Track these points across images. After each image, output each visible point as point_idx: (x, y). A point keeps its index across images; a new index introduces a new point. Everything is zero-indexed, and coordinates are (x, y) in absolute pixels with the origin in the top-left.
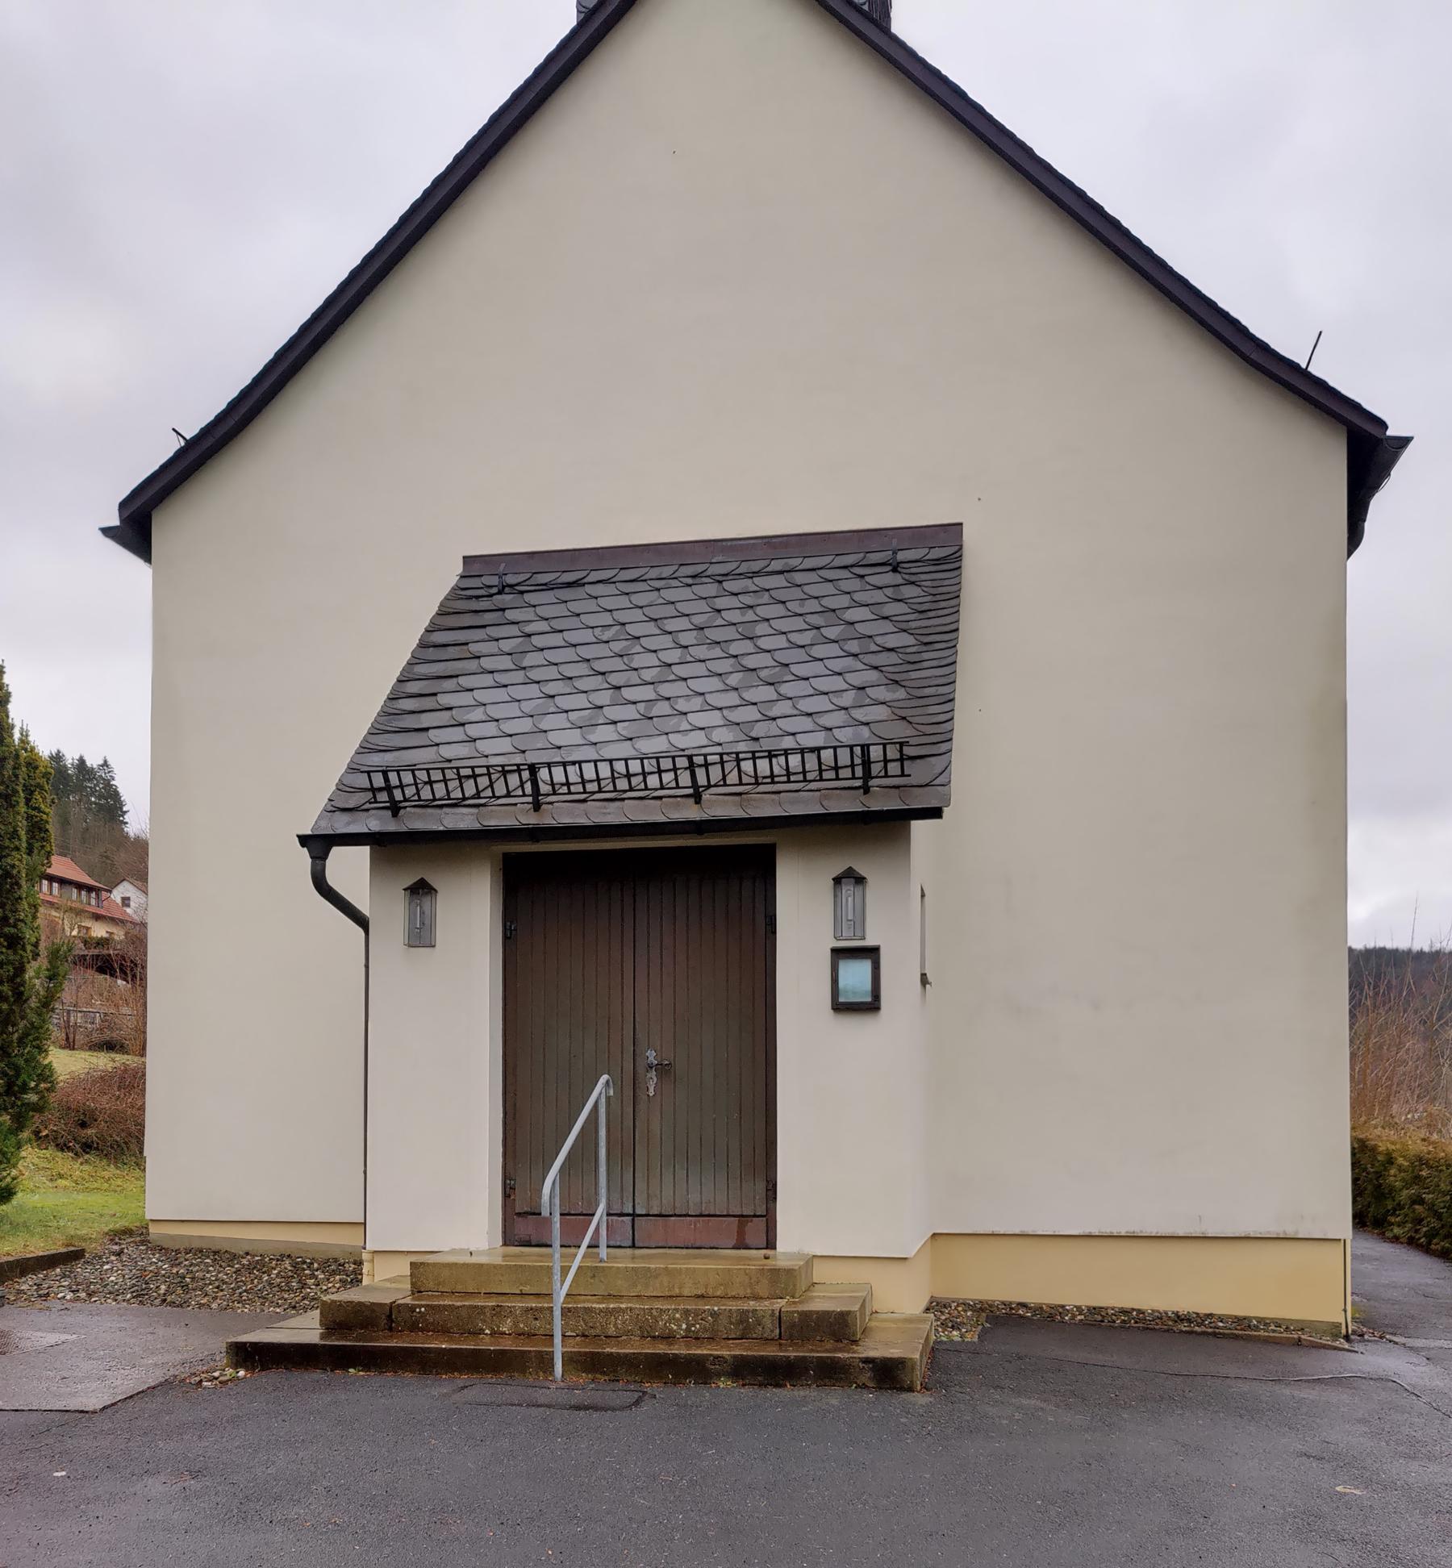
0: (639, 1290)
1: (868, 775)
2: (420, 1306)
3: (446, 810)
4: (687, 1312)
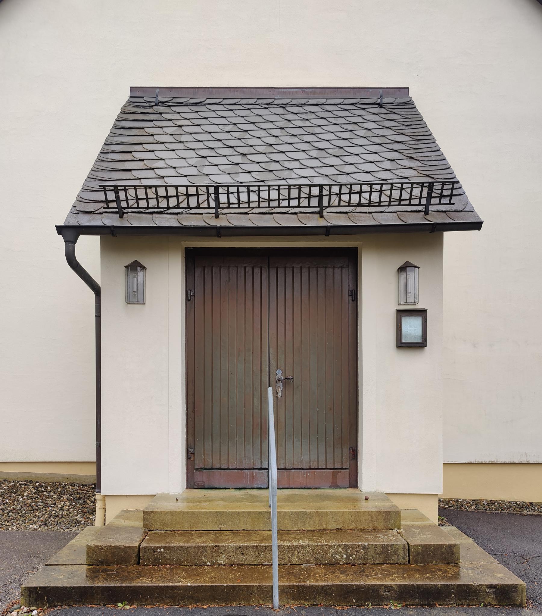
0: (300, 526)
1: (428, 203)
2: (160, 548)
3: (154, 215)
4: (346, 547)
